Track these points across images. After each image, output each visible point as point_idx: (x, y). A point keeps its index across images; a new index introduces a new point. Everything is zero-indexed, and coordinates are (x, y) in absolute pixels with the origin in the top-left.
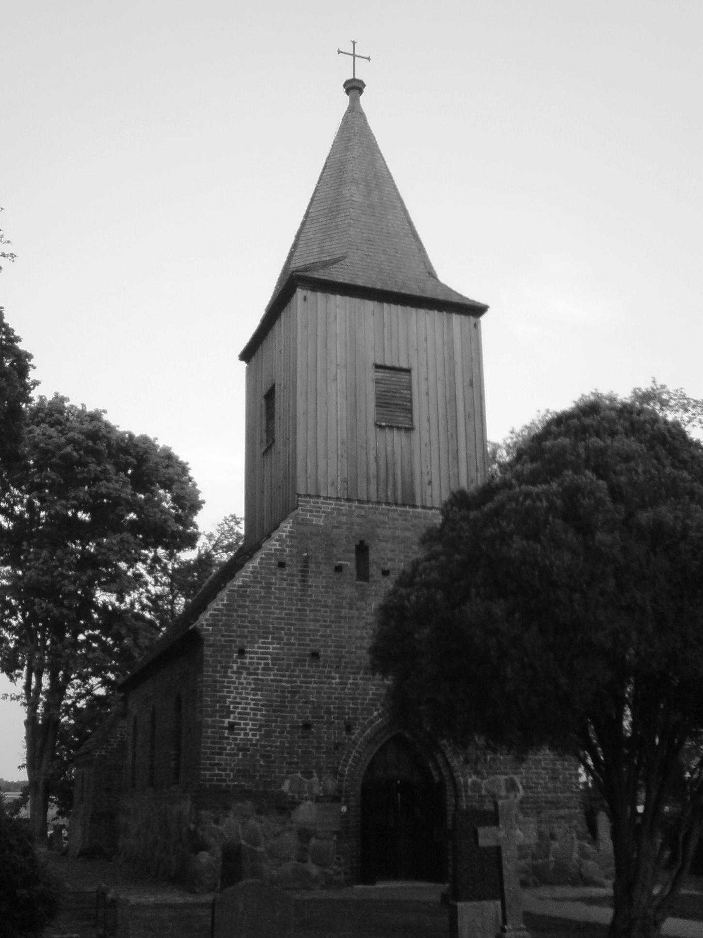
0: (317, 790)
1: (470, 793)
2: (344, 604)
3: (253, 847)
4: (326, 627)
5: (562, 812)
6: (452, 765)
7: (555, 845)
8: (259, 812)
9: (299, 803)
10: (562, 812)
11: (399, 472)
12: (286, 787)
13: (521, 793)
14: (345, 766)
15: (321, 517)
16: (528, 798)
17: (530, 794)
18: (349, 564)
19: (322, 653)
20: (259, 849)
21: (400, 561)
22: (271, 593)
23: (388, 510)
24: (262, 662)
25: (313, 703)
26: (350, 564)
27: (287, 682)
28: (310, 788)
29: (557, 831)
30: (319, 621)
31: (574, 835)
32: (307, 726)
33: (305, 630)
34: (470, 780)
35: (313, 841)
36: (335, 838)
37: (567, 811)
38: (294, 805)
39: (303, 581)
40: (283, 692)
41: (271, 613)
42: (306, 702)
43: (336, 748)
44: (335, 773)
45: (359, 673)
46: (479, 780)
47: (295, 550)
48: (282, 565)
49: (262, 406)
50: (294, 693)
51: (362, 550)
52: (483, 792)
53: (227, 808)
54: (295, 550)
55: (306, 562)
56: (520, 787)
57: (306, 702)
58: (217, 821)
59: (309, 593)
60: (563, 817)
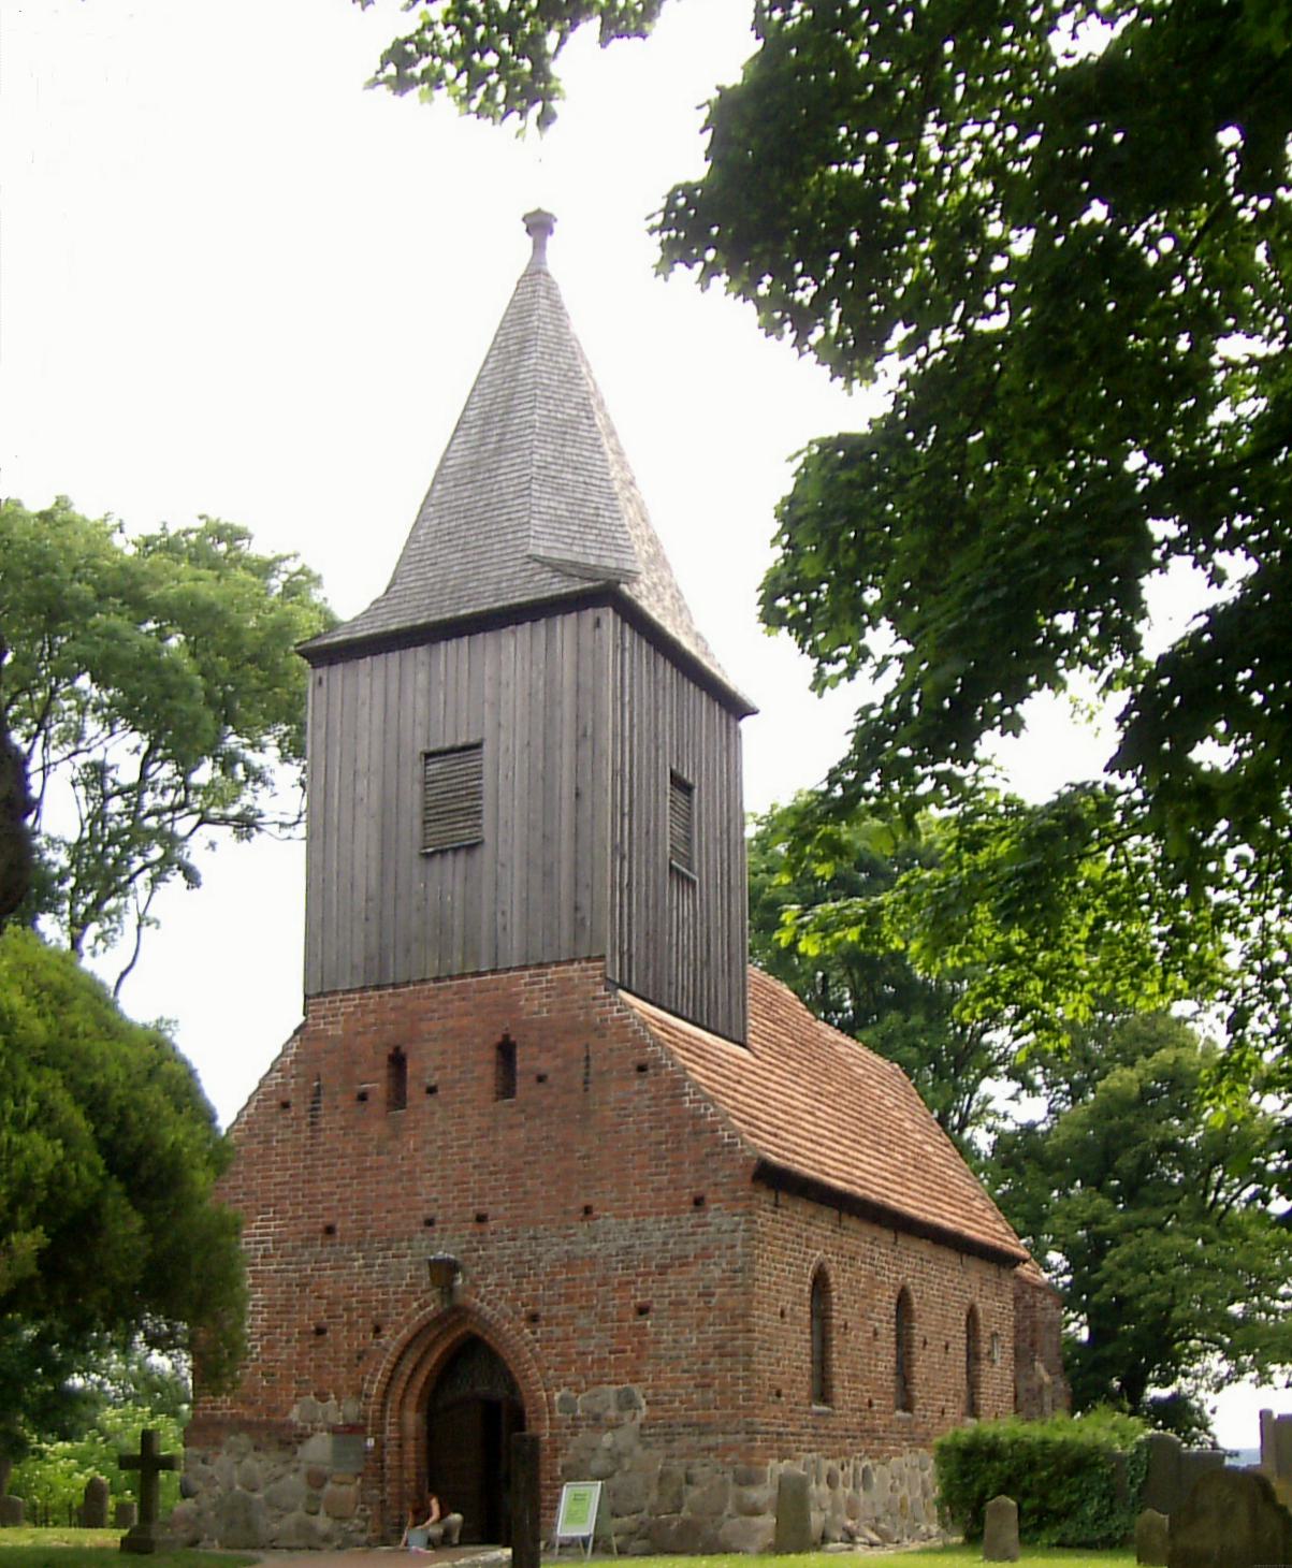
0: (337, 1419)
1: (558, 1414)
2: (370, 1148)
3: (249, 1494)
4: (345, 1186)
5: (711, 1440)
6: (389, 1367)
7: (693, 1493)
8: (256, 1449)
9: (309, 1436)
10: (711, 1440)
11: (457, 922)
12: (295, 1414)
13: (645, 1411)
14: (372, 1382)
15: (338, 1022)
16: (655, 1419)
17: (660, 1414)
18: (377, 1085)
19: (338, 1226)
20: (257, 1496)
21: (454, 1067)
22: (273, 1148)
23: (439, 989)
24: (261, 1246)
25: (327, 1298)
26: (378, 1087)
27: (295, 1271)
28: (325, 1414)
29: (697, 1470)
30: (334, 1179)
31: (729, 1476)
32: (320, 1331)
33: (314, 1195)
34: (557, 1396)
35: (329, 1487)
36: (359, 1481)
37: (720, 1439)
38: (303, 1437)
39: (312, 1123)
40: (289, 1285)
41: (271, 1177)
42: (319, 1297)
43: (359, 1358)
44: (359, 1393)
45: (389, 1249)
46: (573, 1395)
47: (301, 1080)
48: (285, 1105)
49: (368, 837)
50: (302, 1286)
51: (397, 1061)
52: (579, 1413)
53: (218, 1443)
54: (301, 1080)
55: (318, 1094)
56: (643, 1402)
57: (319, 1297)
58: (204, 1461)
59: (322, 1140)
60: (709, 1449)
